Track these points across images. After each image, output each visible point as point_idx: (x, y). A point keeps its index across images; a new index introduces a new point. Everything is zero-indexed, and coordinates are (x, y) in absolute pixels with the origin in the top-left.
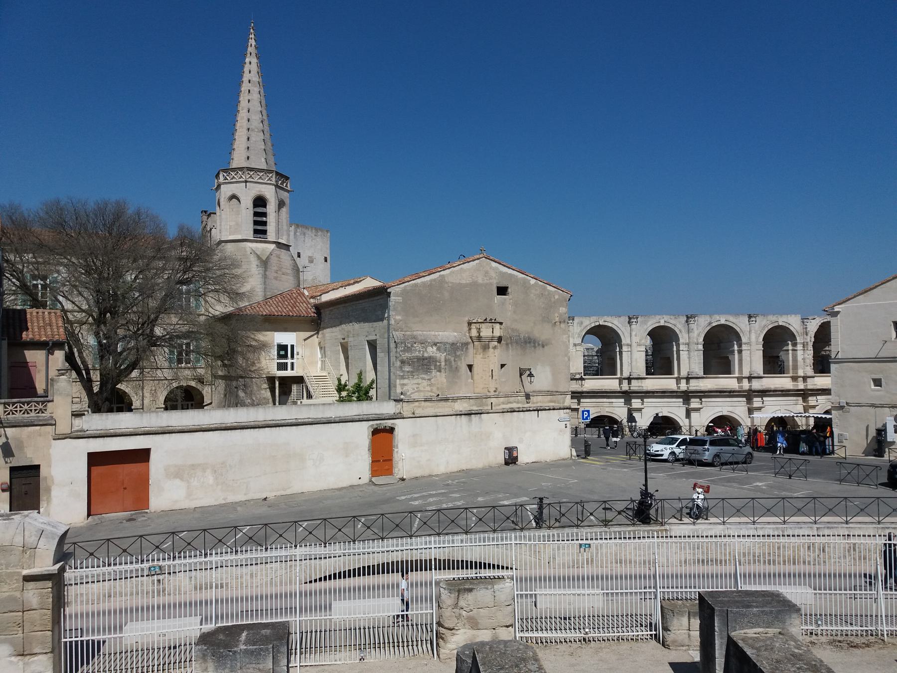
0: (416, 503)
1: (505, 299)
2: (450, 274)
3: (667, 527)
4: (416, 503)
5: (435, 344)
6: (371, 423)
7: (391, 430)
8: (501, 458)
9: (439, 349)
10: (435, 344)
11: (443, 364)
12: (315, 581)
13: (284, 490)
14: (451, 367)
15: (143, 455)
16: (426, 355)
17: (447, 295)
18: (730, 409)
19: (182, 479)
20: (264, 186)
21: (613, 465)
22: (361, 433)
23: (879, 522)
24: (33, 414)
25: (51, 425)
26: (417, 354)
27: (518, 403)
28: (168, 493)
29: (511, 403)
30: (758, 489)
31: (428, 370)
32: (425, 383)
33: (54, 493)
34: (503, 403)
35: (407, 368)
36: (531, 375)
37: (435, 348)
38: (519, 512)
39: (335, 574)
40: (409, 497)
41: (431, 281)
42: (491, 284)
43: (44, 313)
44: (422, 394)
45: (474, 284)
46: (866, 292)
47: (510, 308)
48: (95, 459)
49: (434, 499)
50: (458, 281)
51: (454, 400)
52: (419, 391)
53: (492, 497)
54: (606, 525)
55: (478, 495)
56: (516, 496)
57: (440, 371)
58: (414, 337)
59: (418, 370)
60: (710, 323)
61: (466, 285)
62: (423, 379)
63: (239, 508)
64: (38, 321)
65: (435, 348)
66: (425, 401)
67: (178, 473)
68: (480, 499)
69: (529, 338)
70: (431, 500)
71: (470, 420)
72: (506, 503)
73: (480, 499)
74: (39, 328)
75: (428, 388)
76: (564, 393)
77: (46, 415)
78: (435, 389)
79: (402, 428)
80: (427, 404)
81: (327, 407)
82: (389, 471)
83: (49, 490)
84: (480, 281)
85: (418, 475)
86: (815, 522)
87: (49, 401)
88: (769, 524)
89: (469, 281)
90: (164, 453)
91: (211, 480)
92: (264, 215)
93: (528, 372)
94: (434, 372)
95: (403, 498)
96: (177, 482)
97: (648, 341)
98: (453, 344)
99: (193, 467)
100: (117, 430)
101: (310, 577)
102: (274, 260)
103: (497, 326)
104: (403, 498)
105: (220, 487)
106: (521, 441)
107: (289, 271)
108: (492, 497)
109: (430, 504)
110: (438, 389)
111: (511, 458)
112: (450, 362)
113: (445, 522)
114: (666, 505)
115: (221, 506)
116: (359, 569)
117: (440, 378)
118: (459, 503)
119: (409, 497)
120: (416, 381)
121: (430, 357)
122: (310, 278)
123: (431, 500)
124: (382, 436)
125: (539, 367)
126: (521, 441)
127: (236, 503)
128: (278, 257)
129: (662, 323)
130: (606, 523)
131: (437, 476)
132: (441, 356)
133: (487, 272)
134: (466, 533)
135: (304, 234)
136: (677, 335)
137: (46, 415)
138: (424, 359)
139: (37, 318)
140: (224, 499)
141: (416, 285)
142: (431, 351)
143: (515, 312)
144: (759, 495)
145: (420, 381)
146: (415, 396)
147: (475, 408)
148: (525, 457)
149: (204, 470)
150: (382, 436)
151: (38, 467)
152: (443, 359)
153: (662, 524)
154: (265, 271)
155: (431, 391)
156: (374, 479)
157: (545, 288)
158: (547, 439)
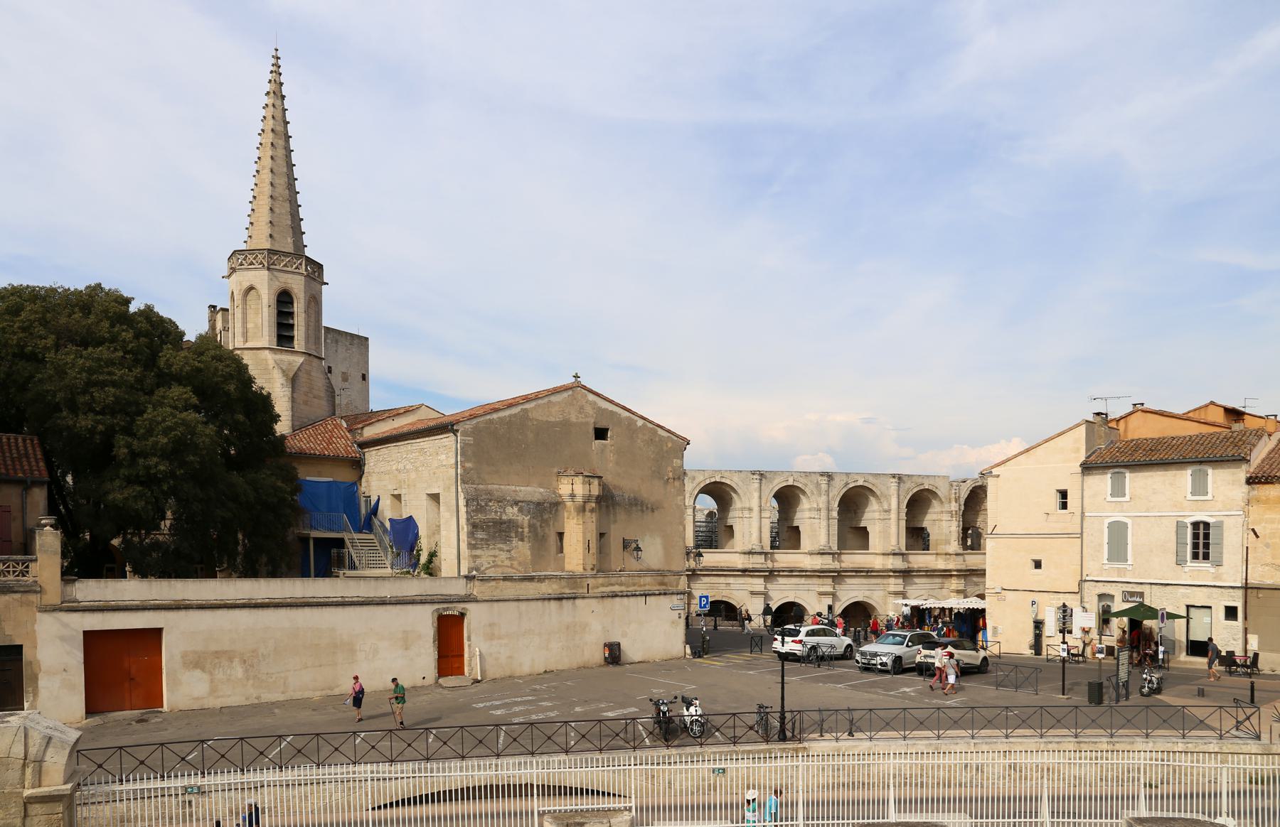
0: (499, 712)
1: (605, 446)
2: (534, 408)
3: (806, 744)
4: (499, 712)
5: (516, 503)
6: (436, 606)
7: (157, 633)
8: (598, 655)
9: (520, 510)
10: (516, 503)
11: (526, 530)
12: (379, 807)
13: (331, 689)
14: (536, 535)
15: (157, 633)
16: (504, 517)
17: (530, 436)
18: (867, 593)
19: (203, 670)
20: (290, 276)
21: (737, 666)
22: (423, 621)
23: (1042, 736)
24: (11, 577)
25: (36, 592)
26: (493, 516)
27: (621, 584)
28: (182, 688)
29: (612, 585)
30: (905, 696)
31: (506, 539)
32: (503, 555)
33: (42, 682)
34: (603, 585)
35: (480, 535)
36: (638, 549)
37: (516, 509)
38: (630, 728)
39: (403, 800)
40: (488, 704)
41: (510, 416)
42: (587, 423)
43: (16, 439)
44: (500, 570)
45: (566, 424)
46: (1028, 450)
47: (612, 457)
48: (91, 638)
49: (521, 708)
50: (545, 419)
51: (541, 579)
52: (496, 566)
53: (593, 706)
54: (735, 743)
55: (574, 704)
56: (623, 706)
57: (522, 540)
58: (489, 493)
59: (494, 537)
60: (847, 484)
61: (555, 424)
62: (501, 550)
63: (276, 711)
64: (10, 451)
65: (516, 509)
66: (505, 579)
67: (196, 662)
68: (578, 709)
69: (635, 499)
70: (517, 709)
71: (561, 607)
72: (610, 714)
73: (578, 709)
74: (13, 459)
75: (507, 563)
76: (678, 574)
77: (29, 579)
78: (515, 563)
79: (476, 618)
80: (508, 584)
81: (380, 582)
82: (459, 671)
83: (35, 678)
84: (573, 419)
85: (497, 676)
86: (973, 737)
87: (31, 561)
88: (922, 742)
89: (559, 418)
90: (180, 636)
91: (239, 672)
92: (291, 314)
93: (634, 545)
94: (515, 542)
95: (481, 705)
96: (198, 673)
97: (775, 504)
98: (539, 504)
99: (217, 654)
100: (126, 599)
101: (373, 802)
102: (303, 377)
103: (596, 482)
104: (481, 705)
105: (251, 682)
106: (624, 635)
107: (322, 394)
108: (593, 706)
109: (516, 714)
110: (520, 564)
111: (614, 655)
112: (536, 529)
113: (536, 738)
114: (805, 717)
115: (254, 706)
116: (433, 794)
117: (523, 549)
118: (552, 714)
119: (488, 704)
120: (492, 553)
121: (510, 521)
122: (344, 402)
123: (517, 709)
124: (449, 634)
125: (647, 538)
126: (624, 635)
127: (273, 703)
128: (308, 373)
129: (790, 483)
130: (735, 741)
131: (520, 677)
132: (524, 520)
133: (582, 408)
134: (567, 752)
135: (337, 342)
136: (715, 483)
137: (29, 579)
138: (502, 522)
139: (9, 445)
140: (258, 698)
141: (491, 421)
142: (512, 512)
143: (617, 463)
144: (907, 704)
145: (497, 552)
146: (490, 573)
147: (567, 591)
148: (632, 651)
149: (231, 660)
150: (449, 634)
151: (21, 646)
152: (526, 524)
153: (800, 741)
154: (293, 392)
155: (512, 567)
156: (441, 680)
157: (656, 432)
158: (655, 631)
